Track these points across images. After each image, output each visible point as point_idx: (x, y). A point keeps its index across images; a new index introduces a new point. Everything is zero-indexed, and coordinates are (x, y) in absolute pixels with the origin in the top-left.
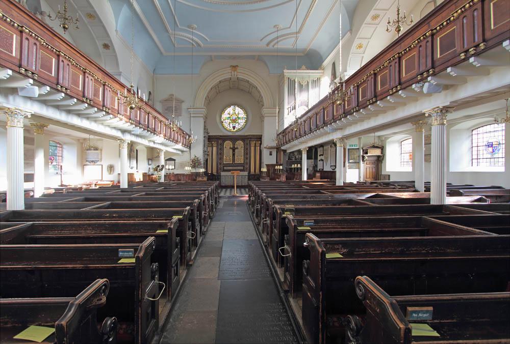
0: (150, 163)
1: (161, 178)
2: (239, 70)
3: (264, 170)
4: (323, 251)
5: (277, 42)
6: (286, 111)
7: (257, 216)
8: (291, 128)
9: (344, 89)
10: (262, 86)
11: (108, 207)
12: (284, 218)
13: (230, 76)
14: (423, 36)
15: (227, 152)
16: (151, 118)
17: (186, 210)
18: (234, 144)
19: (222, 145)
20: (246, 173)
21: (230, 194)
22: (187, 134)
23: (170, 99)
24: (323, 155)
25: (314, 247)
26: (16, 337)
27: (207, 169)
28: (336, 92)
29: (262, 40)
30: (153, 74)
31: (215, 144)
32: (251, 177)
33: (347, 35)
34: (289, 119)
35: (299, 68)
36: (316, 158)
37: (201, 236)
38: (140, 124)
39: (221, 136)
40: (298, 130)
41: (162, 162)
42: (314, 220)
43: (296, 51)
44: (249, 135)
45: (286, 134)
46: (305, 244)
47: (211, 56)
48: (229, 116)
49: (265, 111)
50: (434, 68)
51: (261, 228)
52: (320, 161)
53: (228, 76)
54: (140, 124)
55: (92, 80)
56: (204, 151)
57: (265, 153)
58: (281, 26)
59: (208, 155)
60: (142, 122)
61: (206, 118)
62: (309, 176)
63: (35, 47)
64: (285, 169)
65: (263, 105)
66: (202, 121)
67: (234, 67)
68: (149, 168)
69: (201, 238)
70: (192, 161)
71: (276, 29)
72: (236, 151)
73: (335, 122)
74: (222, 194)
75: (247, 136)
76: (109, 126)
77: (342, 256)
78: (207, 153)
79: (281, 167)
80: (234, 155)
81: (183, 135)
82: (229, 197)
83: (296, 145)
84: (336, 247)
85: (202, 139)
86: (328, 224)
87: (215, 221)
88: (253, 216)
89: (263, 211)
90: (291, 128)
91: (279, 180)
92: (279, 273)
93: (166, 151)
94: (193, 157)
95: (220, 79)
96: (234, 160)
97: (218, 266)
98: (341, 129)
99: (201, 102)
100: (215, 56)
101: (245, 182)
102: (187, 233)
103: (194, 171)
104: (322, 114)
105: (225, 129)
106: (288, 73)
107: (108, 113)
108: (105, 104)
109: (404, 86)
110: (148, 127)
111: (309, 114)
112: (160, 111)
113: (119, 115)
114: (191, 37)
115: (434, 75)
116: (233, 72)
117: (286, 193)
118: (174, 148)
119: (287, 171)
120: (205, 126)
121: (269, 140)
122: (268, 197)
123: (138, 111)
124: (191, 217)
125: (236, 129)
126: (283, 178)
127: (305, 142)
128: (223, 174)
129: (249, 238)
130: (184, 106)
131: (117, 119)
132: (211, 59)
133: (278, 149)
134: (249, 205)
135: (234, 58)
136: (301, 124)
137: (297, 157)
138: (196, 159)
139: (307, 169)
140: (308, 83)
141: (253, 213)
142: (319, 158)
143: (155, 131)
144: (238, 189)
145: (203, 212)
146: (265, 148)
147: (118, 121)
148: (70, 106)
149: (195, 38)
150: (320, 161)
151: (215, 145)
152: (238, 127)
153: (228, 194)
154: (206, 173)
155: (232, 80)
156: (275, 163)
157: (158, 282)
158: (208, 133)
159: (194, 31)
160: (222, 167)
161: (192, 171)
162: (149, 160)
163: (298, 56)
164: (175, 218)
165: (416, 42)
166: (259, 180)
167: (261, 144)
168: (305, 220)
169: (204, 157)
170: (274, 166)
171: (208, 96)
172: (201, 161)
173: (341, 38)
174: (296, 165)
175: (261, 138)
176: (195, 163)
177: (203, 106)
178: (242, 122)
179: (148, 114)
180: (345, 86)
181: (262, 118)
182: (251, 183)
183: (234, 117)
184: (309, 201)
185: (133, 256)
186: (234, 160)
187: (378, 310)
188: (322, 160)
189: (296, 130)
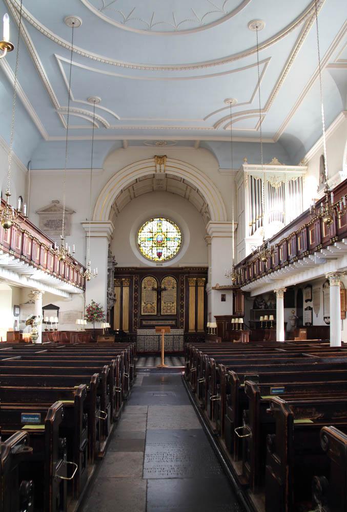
0: (17, 311)
1: (37, 338)
2: (169, 162)
3: (213, 325)
5: (231, 123)
6: (248, 230)
7: (201, 396)
8: (256, 256)
9: (332, 201)
10: (209, 190)
11: (20, 359)
13: (154, 173)
16: (26, 240)
17: (94, 377)
19: (139, 283)
20: (181, 331)
21: (154, 365)
22: (80, 265)
23: (54, 207)
24: (311, 300)
25: (280, 413)
26: (23, 428)
27: (112, 323)
28: (322, 204)
29: (205, 119)
30: (27, 170)
32: (188, 337)
33: (338, 118)
34: (252, 243)
35: (268, 161)
36: (300, 306)
37: (111, 423)
38: (10, 249)
39: (136, 269)
40: (268, 260)
41: (39, 311)
42: (284, 385)
43: (261, 136)
45: (249, 266)
46: (269, 409)
47: (122, 141)
48: (150, 235)
49: (212, 228)
51: (207, 413)
52: (306, 309)
53: (150, 172)
54: (10, 249)
56: (108, 294)
57: (214, 297)
58: (236, 100)
60: (13, 246)
61: (111, 239)
62: (288, 335)
64: (248, 324)
65: (209, 219)
66: (105, 243)
67: (161, 158)
68: (16, 321)
69: (113, 425)
70: (88, 311)
71: (228, 105)
72: (164, 293)
73: (324, 248)
74: (140, 365)
75: (182, 268)
77: (312, 422)
78: (112, 297)
79: (241, 321)
80: (159, 301)
81: (73, 266)
82: (152, 370)
83: (266, 285)
84: (308, 411)
85: (105, 273)
86: (305, 391)
87: (130, 405)
88: (194, 397)
89: (210, 386)
90: (256, 256)
91: (238, 341)
92: (235, 467)
93: (46, 292)
94: (89, 303)
95: (137, 177)
96: (159, 309)
97: (141, 463)
98: (336, 259)
99: (104, 211)
100: (128, 141)
101: (180, 345)
102: (96, 412)
103: (90, 326)
104: (305, 234)
105: (144, 257)
106: (249, 168)
110: (22, 254)
111: (285, 235)
112: (36, 224)
114: (92, 113)
116: (158, 166)
117: (249, 357)
118: (60, 289)
119: (251, 327)
120: (110, 252)
121: (221, 274)
122: (218, 363)
124: (89, 402)
125: (162, 258)
126: (245, 339)
127: (282, 279)
129: (187, 428)
130: (76, 219)
132: (122, 145)
133: (236, 290)
134: (188, 380)
135: (161, 143)
136: (273, 251)
137: (269, 304)
138: (94, 307)
139: (285, 324)
140: (283, 184)
141: (194, 392)
142: (305, 305)
143: (31, 260)
144: (167, 358)
145: (115, 387)
146: (213, 288)
149: (97, 116)
150: (306, 309)
152: (166, 253)
153: (150, 365)
154: (110, 331)
155: (157, 177)
156: (231, 313)
157: (67, 462)
158: (114, 264)
159: (96, 105)
160: (138, 320)
161: (87, 328)
162: (15, 307)
163: (263, 143)
164: (58, 404)
166: (204, 342)
167: (206, 282)
168: (273, 386)
169: (108, 303)
170: (228, 318)
171: (115, 203)
172: (103, 310)
173: (324, 129)
174: (266, 317)
176: (93, 314)
177: (106, 220)
178: (172, 247)
179: (23, 233)
180: (334, 196)
181: (207, 240)
182: (190, 346)
183: (160, 237)
184: (281, 367)
185: (39, 421)
186: (159, 309)
187: (339, 455)
188: (310, 309)
189: (265, 261)
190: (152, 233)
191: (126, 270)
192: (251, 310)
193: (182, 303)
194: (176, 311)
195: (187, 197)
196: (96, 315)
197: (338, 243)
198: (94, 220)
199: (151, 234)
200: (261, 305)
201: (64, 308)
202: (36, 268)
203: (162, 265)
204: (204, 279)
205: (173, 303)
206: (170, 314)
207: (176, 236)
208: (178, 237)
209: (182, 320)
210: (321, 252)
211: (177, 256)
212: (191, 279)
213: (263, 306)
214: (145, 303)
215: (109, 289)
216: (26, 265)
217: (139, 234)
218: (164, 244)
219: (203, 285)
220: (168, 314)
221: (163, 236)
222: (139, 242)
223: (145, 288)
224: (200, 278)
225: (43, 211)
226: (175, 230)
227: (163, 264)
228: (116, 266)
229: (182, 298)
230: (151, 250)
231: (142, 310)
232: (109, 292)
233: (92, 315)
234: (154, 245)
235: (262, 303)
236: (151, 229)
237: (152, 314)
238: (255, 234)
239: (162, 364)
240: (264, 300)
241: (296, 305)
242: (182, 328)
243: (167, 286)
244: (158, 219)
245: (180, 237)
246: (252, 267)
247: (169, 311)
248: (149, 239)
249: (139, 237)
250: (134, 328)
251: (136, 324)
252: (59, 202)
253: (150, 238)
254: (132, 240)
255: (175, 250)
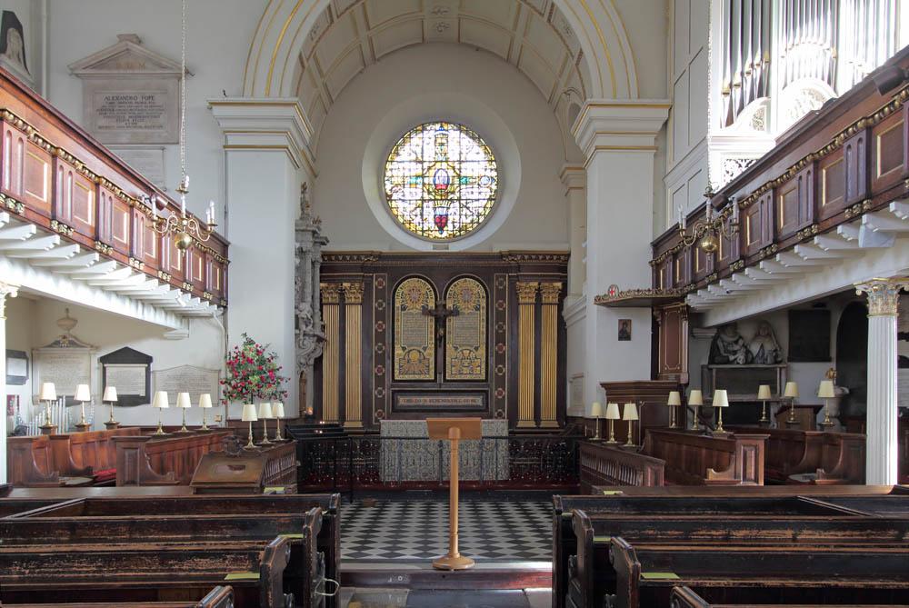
4: (635, 566)
6: (717, 108)
12: (569, 520)
14: (888, 106)
15: (412, 346)
18: (441, 294)
20: (499, 426)
31: (353, 292)
34: (734, 143)
39: (380, 256)
44: (511, 254)
48: (417, 169)
50: (818, 224)
55: (21, 140)
59: (320, 340)
63: (70, 178)
70: (233, 364)
72: (452, 323)
75: (501, 256)
76: (102, 288)
80: (440, 341)
94: (236, 342)
96: (440, 366)
99: (277, 74)
107: (106, 257)
108: (135, 252)
109: (784, 246)
112: (74, 116)
113: (131, 260)
115: (873, 210)
121: (613, 257)
123: (126, 216)
128: (389, 427)
130: (193, 95)
131: (128, 270)
137: (755, 349)
138: (250, 355)
147: (56, 246)
148: (19, 241)
151: (354, 295)
165: (842, 135)
167: (564, 293)
169: (299, 344)
172: (277, 363)
175: (564, 269)
176: (246, 375)
178: (478, 198)
186: (440, 366)
190: (422, 162)
191: (344, 259)
192: (703, 367)
193: (500, 348)
194: (484, 371)
195: (514, 56)
196: (255, 379)
197: (900, 204)
198: (248, 91)
199: (420, 165)
200: (735, 353)
201: (165, 357)
202: (114, 263)
203: (448, 248)
204: (559, 285)
205: (476, 349)
206: (468, 377)
207: (483, 173)
208: (489, 173)
209: (500, 393)
210: (761, 267)
211: (488, 226)
212: (524, 284)
213: (741, 357)
214: (404, 349)
215: (302, 306)
216: (194, 299)
217: (389, 166)
218: (453, 193)
219: (556, 301)
220: (463, 377)
221: (451, 173)
222: (388, 186)
223: (404, 308)
224: (546, 281)
225: (93, 66)
226: (482, 156)
227: (451, 245)
228: (324, 248)
229: (499, 337)
230: (418, 210)
231: (397, 366)
232: (303, 315)
233: (245, 378)
234: (426, 196)
235: (736, 348)
236: (419, 150)
237: (422, 377)
238: (738, 121)
239: (450, 555)
240: (741, 337)
241: (833, 353)
242: (500, 415)
243: (461, 306)
244: (438, 126)
245: (494, 174)
246: (670, 266)
247: (466, 370)
248: (413, 180)
249: (388, 174)
250: (375, 415)
251: (380, 403)
252: (140, 42)
253: (417, 177)
254: (368, 182)
255: (481, 210)
